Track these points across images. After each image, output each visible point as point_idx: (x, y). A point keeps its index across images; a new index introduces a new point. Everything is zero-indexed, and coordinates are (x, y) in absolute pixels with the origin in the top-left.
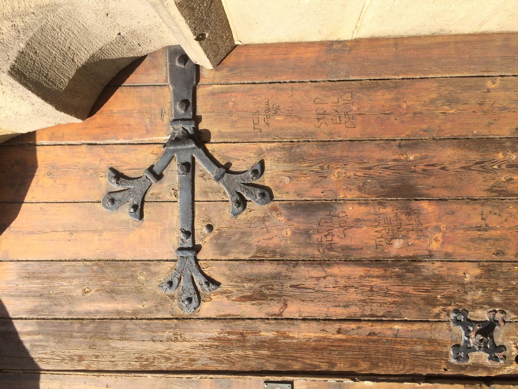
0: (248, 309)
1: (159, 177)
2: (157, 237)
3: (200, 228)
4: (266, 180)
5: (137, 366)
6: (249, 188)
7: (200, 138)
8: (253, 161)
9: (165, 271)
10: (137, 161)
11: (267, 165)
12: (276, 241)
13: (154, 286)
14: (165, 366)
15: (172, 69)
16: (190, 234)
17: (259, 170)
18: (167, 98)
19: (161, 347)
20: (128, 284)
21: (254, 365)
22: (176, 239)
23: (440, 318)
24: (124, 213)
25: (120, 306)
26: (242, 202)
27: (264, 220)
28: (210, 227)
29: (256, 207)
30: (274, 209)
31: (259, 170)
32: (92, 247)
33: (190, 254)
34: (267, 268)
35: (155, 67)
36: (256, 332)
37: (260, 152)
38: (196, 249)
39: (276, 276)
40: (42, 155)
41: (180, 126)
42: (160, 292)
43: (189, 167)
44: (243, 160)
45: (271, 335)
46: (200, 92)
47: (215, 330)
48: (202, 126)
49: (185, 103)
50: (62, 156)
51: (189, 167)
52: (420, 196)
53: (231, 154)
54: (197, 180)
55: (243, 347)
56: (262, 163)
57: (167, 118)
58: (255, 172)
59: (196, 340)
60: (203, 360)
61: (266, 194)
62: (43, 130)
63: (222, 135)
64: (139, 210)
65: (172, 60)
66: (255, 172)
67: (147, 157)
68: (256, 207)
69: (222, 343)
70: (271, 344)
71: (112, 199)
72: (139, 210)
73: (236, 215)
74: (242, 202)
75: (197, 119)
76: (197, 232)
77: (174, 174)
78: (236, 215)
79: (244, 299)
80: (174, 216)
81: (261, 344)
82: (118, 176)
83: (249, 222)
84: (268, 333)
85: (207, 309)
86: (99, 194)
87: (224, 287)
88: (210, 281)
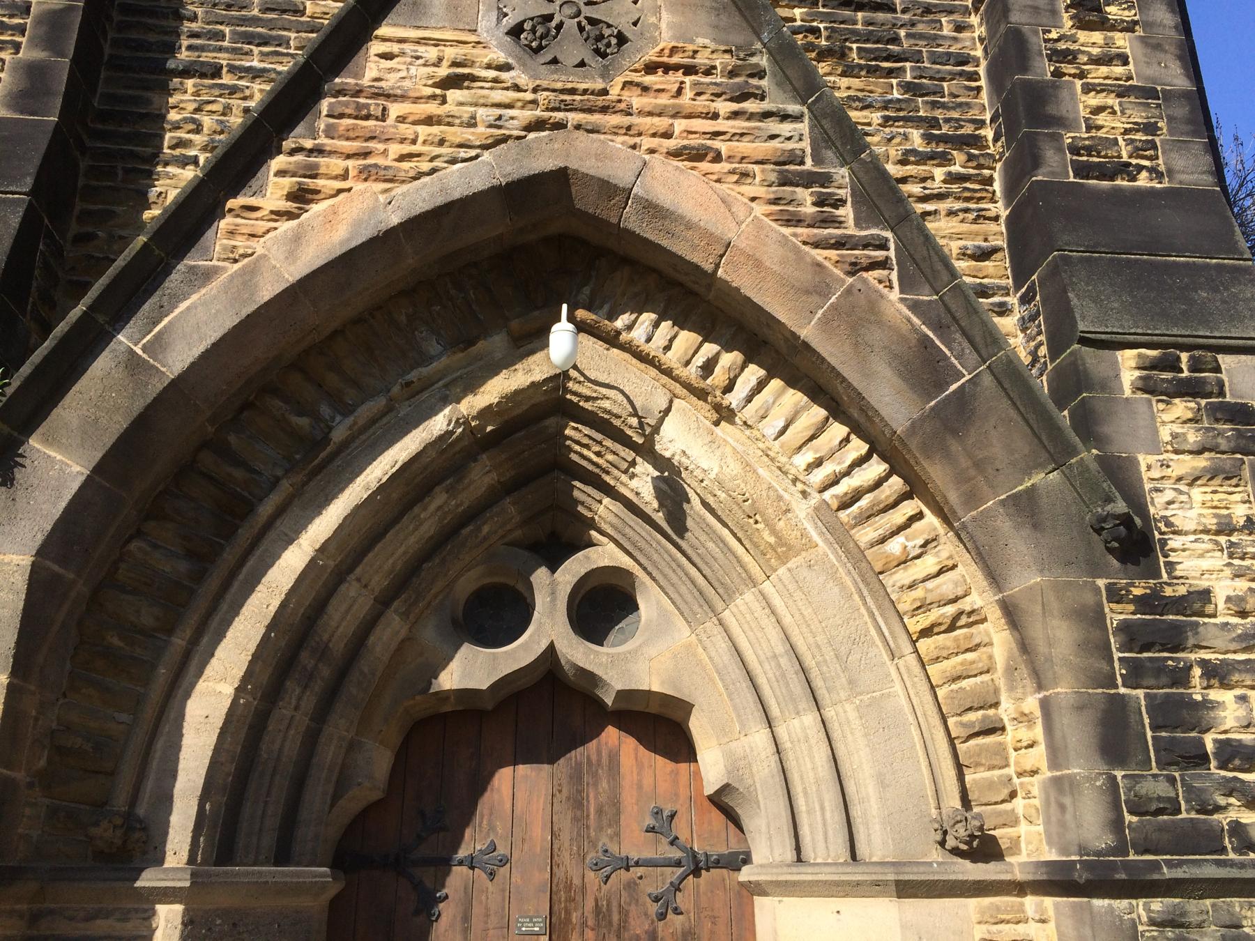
0: (590, 904)
1: (672, 843)
2: (635, 844)
3: (640, 871)
4: (670, 915)
5: (555, 829)
6: (666, 904)
7: (696, 872)
8: (683, 907)
9: (613, 848)
10: (681, 829)
11: (680, 917)
12: (633, 923)
13: (604, 841)
14: (555, 846)
15: (738, 853)
16: (637, 864)
17: (677, 911)
18: (719, 849)
19: (567, 844)
20: (605, 822)
21: (556, 908)
22: (634, 856)
23: (1216, 516)
24: (649, 821)
25: (592, 817)
26: (657, 900)
27: (646, 914)
28: (641, 878)
29: (654, 908)
30: (653, 922)
31: (677, 911)
32: (628, 798)
33: (624, 865)
34: (615, 917)
35: (739, 842)
36: (576, 909)
37: (688, 913)
38: (628, 869)
39: (610, 923)
40: (684, 766)
41: (703, 858)
42: (600, 844)
43: (678, 864)
44: (681, 900)
45: (574, 920)
46: (724, 871)
47: (577, 881)
48: (703, 872)
49: (718, 861)
50: (684, 779)
51: (678, 864)
52: (503, 908)
53: (686, 893)
54: (670, 869)
55: (566, 901)
56: (681, 913)
57: (708, 848)
58: (676, 909)
59: (570, 867)
60: (560, 873)
61: (662, 916)
62: (698, 773)
63: (698, 886)
64: (651, 830)
65: (743, 853)
66: (676, 909)
67: (683, 836)
68: (654, 908)
69: (569, 887)
70: (568, 920)
71: (657, 813)
72: (651, 830)
73: (649, 895)
74: (657, 900)
75: (708, 869)
76: (638, 869)
77: (676, 854)
78: (649, 895)
79: (596, 901)
80: (648, 854)
81: (568, 913)
82: (672, 816)
83: (644, 904)
84: (575, 917)
85: (591, 875)
86: (660, 804)
87: (604, 887)
88: (608, 877)
